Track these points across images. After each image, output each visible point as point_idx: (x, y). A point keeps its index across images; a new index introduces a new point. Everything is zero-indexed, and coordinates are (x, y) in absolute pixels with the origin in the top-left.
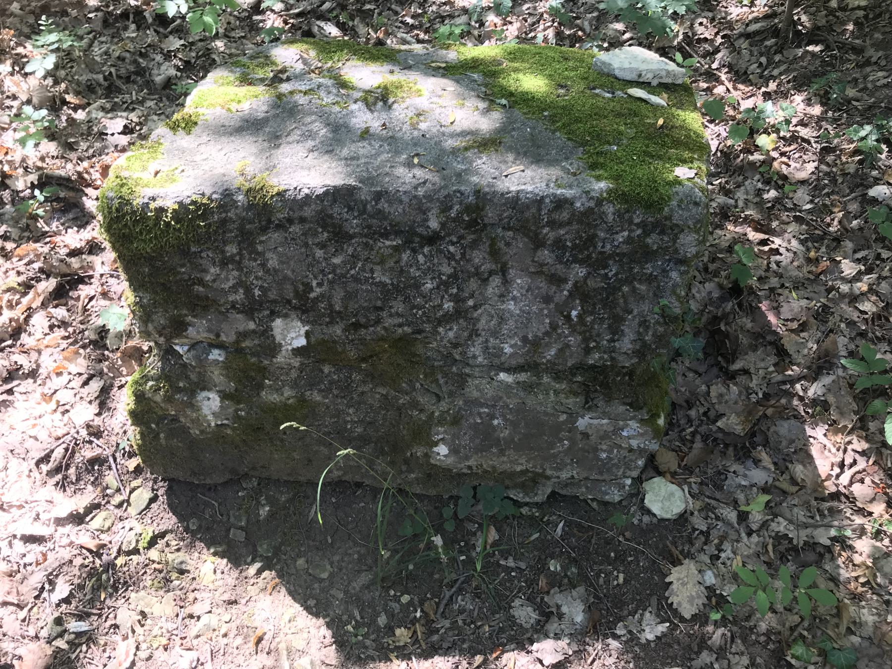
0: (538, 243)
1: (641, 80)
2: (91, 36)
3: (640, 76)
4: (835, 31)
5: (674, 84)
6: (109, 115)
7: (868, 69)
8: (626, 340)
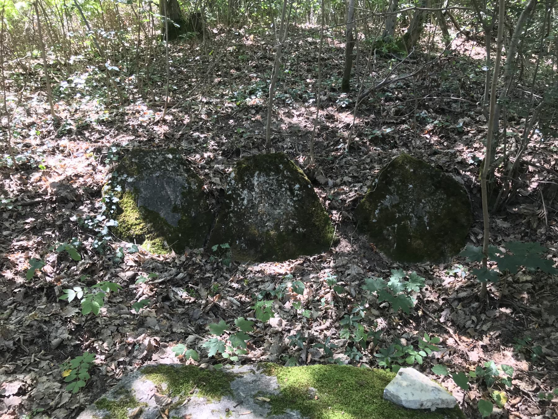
1: (423, 408)
2: (12, 306)
3: (422, 405)
4: (516, 298)
5: (448, 409)
6: (10, 379)
7: (548, 330)
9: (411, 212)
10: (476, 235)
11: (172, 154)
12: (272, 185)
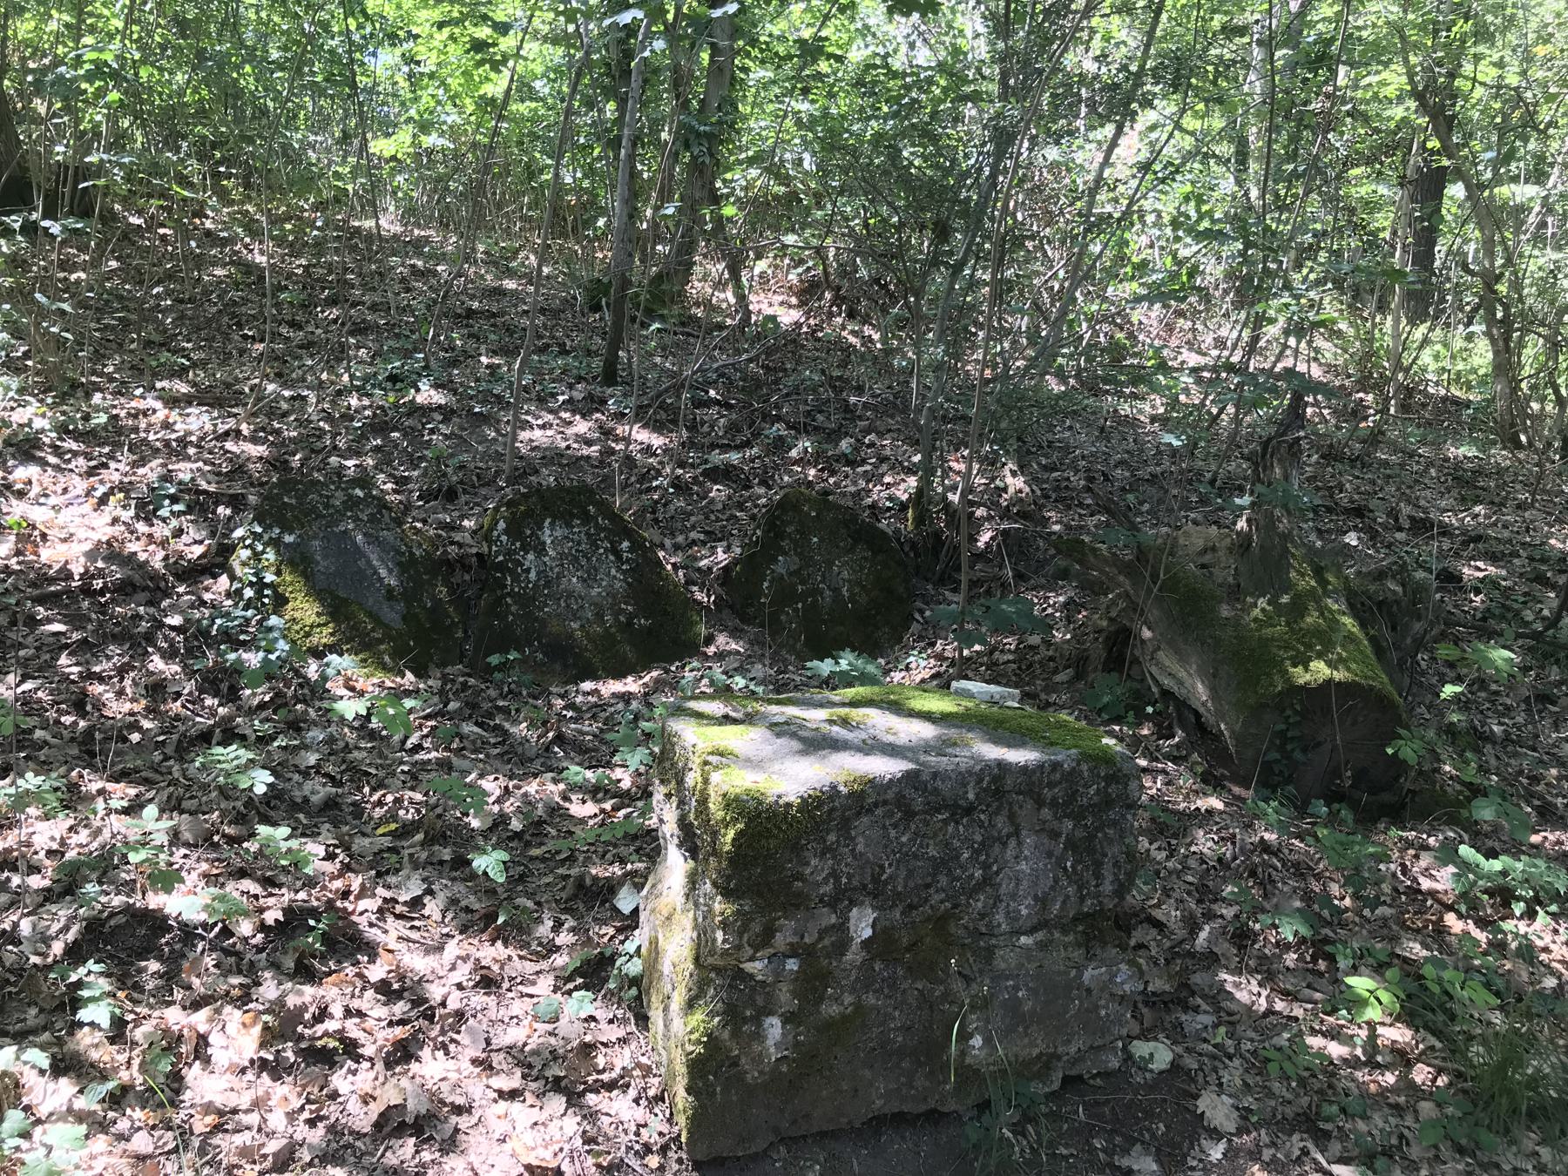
0: (1040, 803)
8: (1107, 882)
9: (822, 582)
10: (921, 612)
11: (362, 488)
12: (579, 544)
